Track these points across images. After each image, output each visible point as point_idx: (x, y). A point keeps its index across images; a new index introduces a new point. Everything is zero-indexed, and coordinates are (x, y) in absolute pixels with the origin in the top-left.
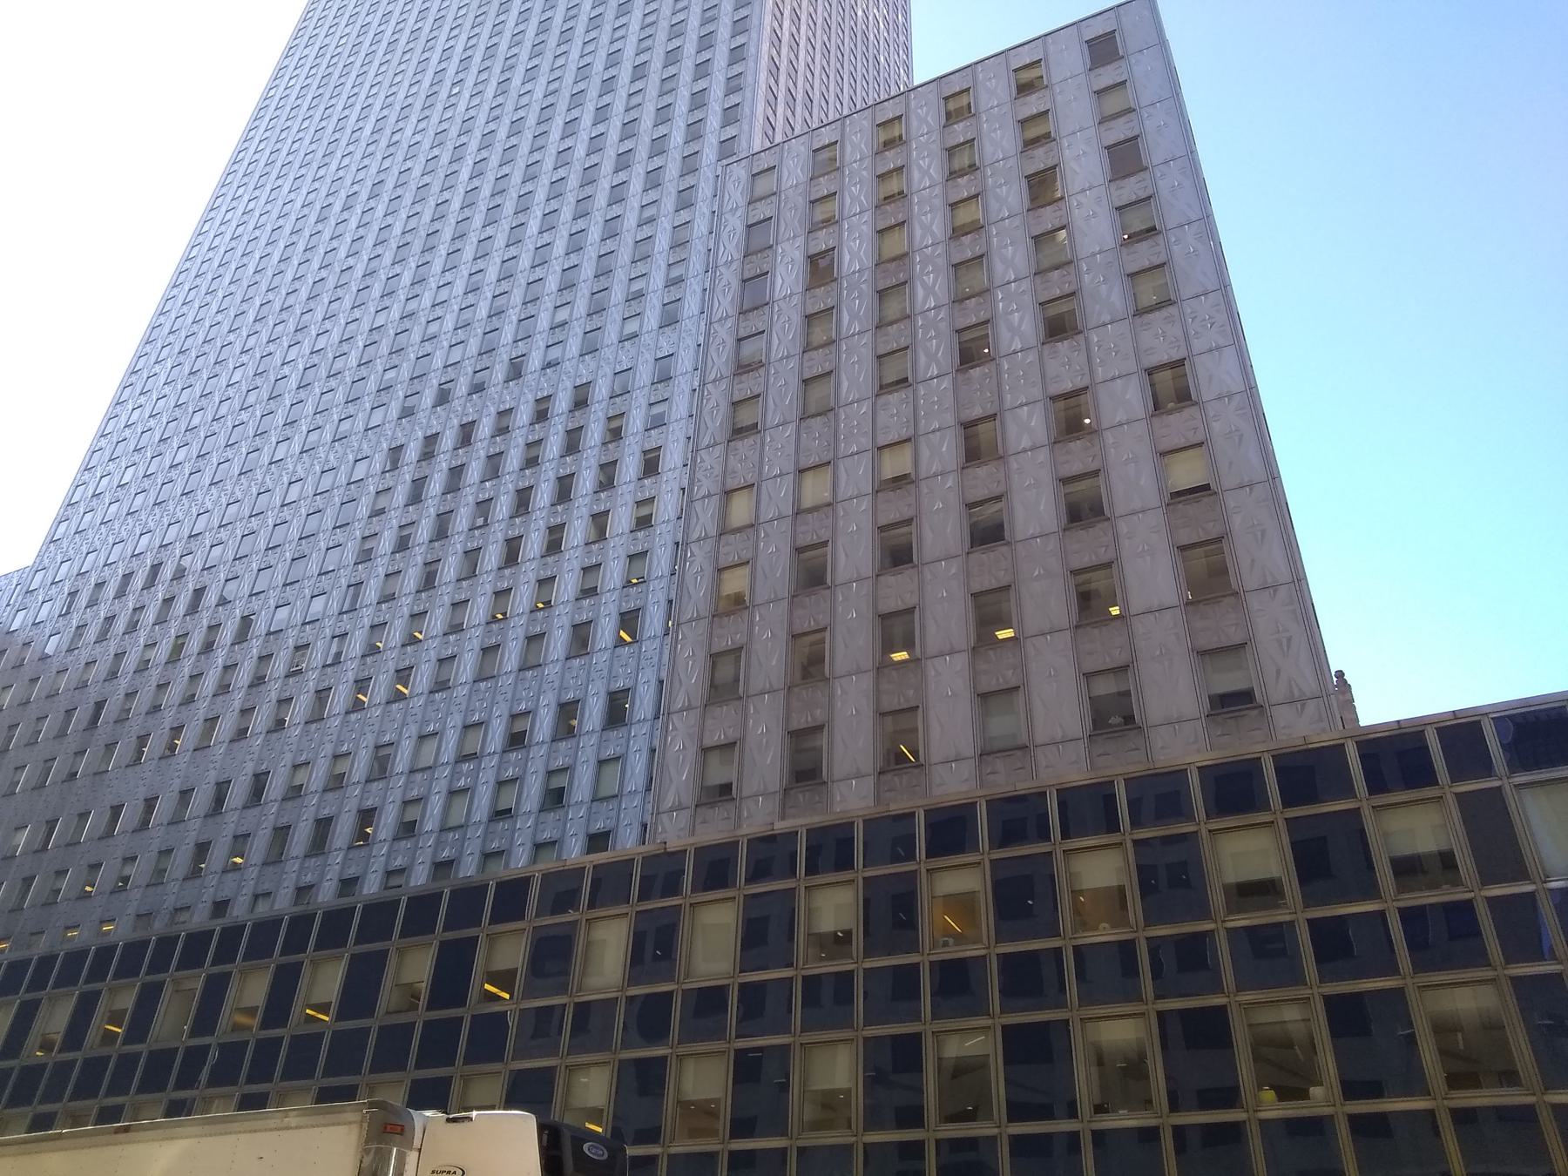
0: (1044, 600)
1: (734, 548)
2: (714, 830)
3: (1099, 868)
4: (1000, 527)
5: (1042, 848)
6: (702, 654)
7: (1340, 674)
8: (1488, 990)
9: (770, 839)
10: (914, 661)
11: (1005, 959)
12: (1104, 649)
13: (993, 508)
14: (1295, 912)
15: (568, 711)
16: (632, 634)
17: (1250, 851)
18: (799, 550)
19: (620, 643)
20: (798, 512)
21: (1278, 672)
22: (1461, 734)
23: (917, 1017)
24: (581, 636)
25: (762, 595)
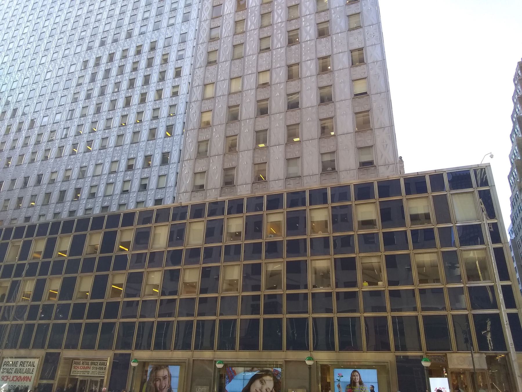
0: (310, 129)
1: (208, 105)
2: (198, 199)
3: (320, 215)
4: (298, 103)
5: (303, 208)
6: (195, 142)
7: (401, 158)
8: (435, 255)
9: (216, 203)
10: (267, 147)
11: (288, 241)
12: (328, 146)
13: (236, 108)
14: (379, 230)
15: (148, 158)
16: (171, 134)
17: (367, 211)
18: (229, 107)
19: (166, 136)
20: (230, 94)
21: (382, 155)
22: (437, 178)
23: (260, 258)
24: (153, 133)
25: (216, 122)
